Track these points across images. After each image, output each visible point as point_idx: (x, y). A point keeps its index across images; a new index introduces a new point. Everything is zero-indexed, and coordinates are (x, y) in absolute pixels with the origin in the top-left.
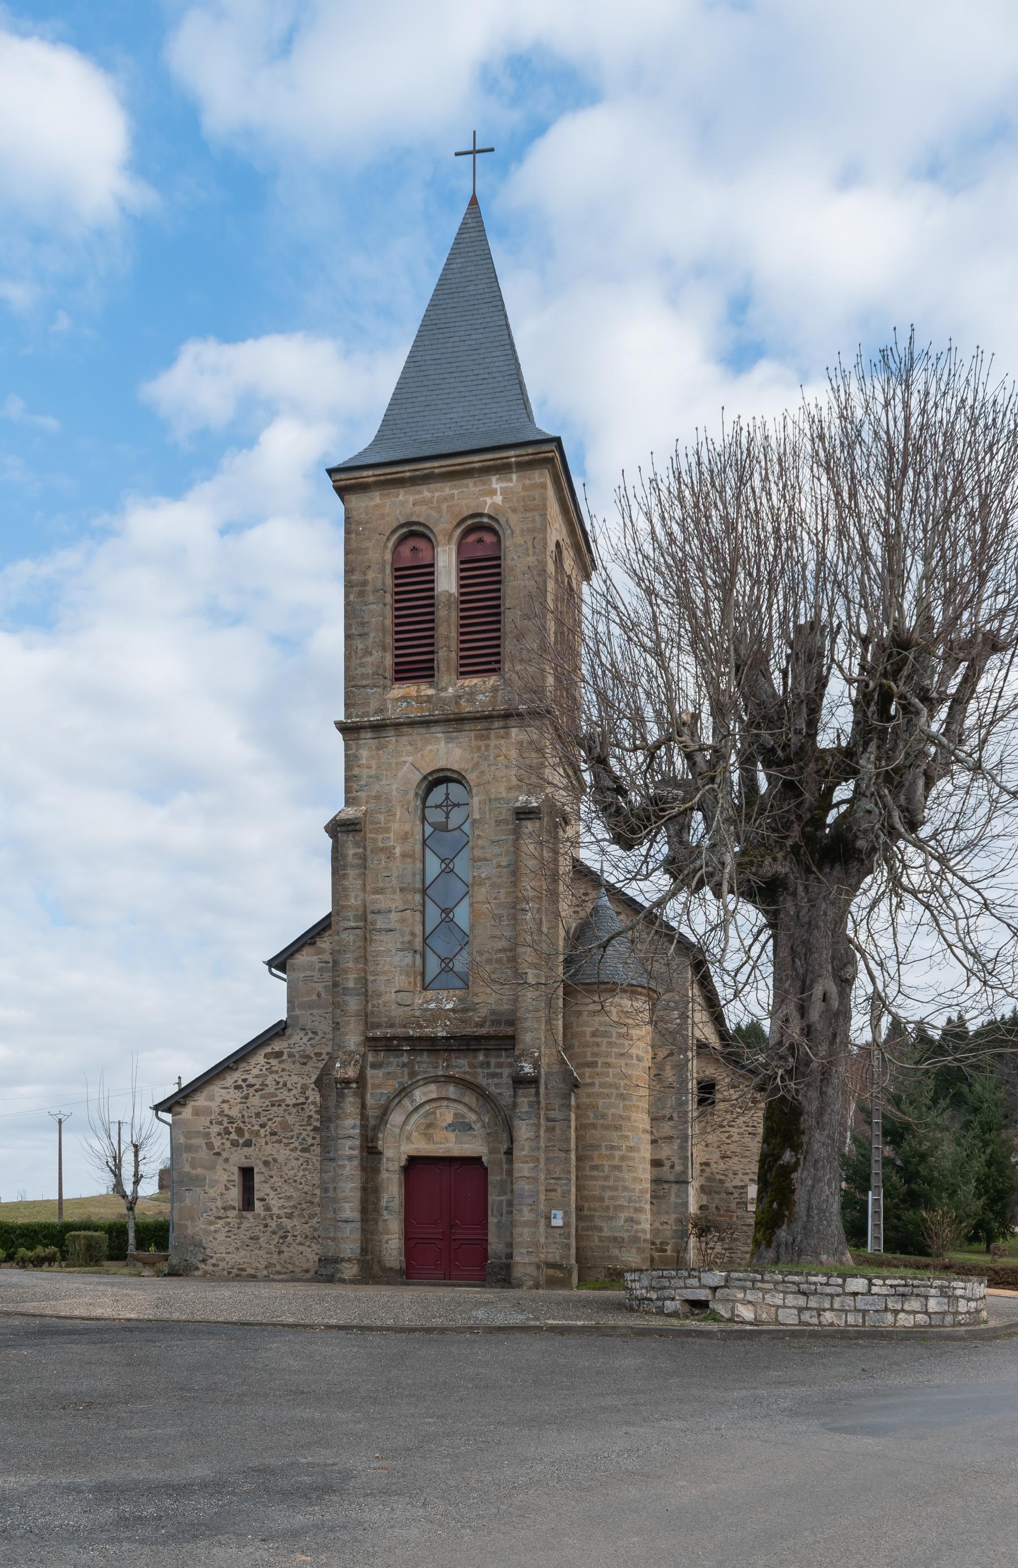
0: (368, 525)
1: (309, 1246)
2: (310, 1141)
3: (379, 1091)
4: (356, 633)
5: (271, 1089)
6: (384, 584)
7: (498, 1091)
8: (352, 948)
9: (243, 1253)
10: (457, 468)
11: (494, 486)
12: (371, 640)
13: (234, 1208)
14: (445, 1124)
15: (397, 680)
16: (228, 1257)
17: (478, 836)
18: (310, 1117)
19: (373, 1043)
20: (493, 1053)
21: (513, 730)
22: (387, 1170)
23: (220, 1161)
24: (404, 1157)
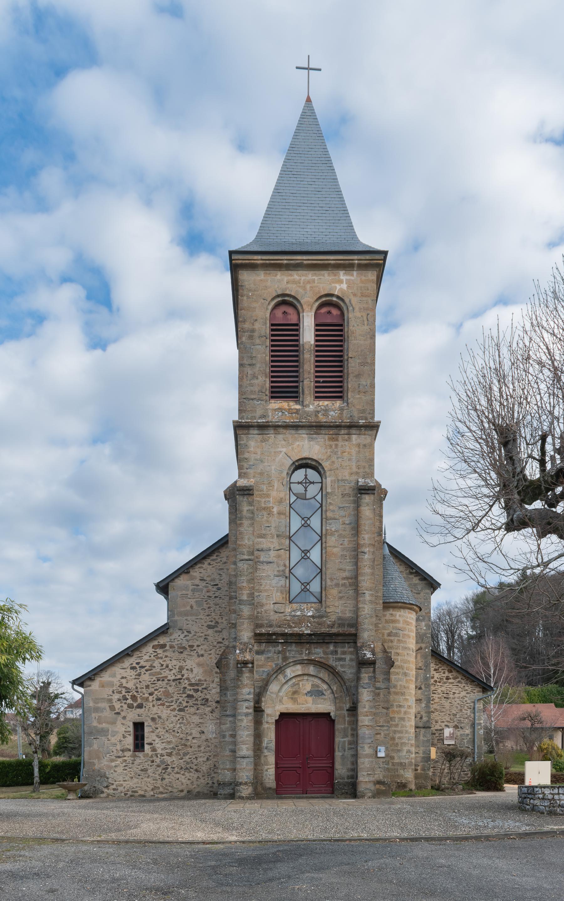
0: (256, 293)
1: (183, 775)
2: (185, 704)
3: (261, 669)
4: (247, 363)
5: (157, 669)
6: (266, 333)
7: (343, 670)
8: (246, 573)
9: (135, 780)
10: (319, 262)
11: (342, 277)
12: (257, 369)
13: (130, 750)
14: (305, 692)
15: (272, 397)
16: (125, 784)
17: (330, 503)
18: (185, 688)
19: (258, 638)
20: (340, 645)
21: (354, 436)
22: (267, 722)
23: (120, 718)
24: (278, 713)
